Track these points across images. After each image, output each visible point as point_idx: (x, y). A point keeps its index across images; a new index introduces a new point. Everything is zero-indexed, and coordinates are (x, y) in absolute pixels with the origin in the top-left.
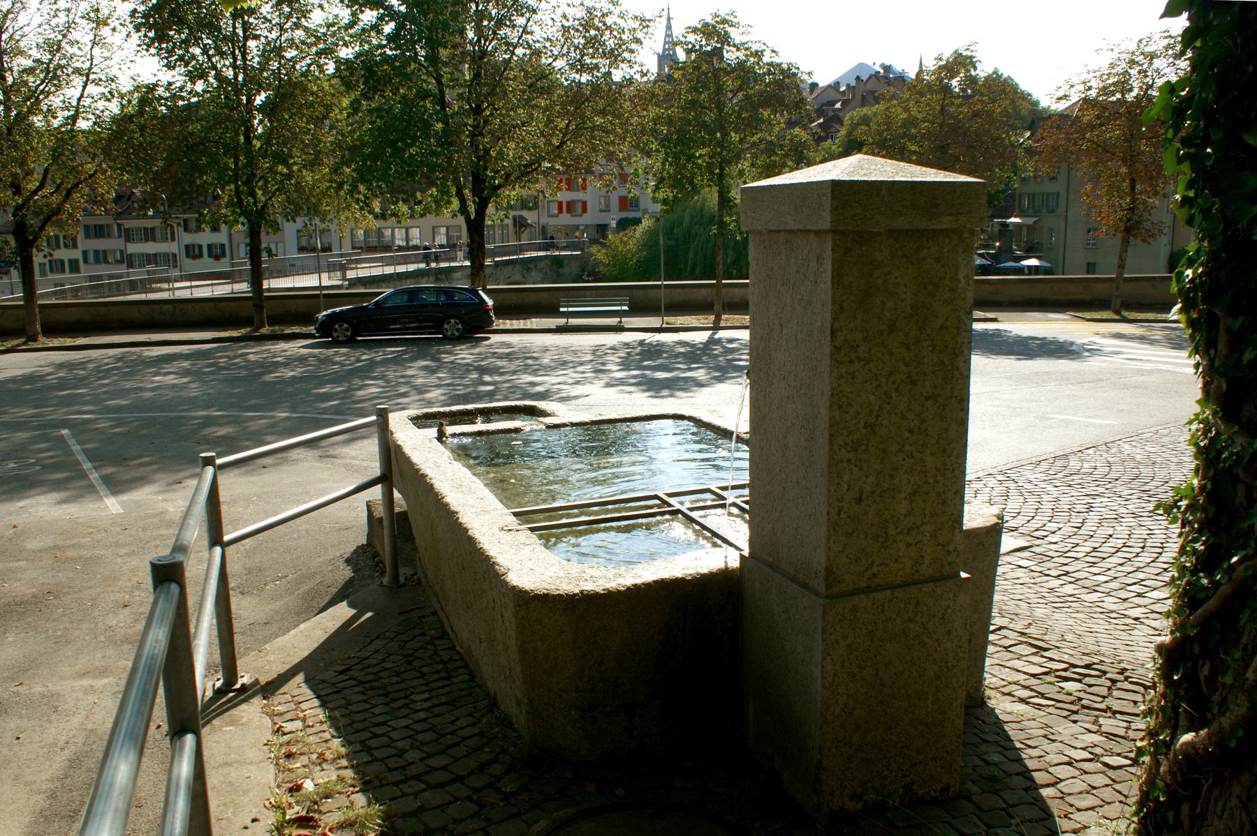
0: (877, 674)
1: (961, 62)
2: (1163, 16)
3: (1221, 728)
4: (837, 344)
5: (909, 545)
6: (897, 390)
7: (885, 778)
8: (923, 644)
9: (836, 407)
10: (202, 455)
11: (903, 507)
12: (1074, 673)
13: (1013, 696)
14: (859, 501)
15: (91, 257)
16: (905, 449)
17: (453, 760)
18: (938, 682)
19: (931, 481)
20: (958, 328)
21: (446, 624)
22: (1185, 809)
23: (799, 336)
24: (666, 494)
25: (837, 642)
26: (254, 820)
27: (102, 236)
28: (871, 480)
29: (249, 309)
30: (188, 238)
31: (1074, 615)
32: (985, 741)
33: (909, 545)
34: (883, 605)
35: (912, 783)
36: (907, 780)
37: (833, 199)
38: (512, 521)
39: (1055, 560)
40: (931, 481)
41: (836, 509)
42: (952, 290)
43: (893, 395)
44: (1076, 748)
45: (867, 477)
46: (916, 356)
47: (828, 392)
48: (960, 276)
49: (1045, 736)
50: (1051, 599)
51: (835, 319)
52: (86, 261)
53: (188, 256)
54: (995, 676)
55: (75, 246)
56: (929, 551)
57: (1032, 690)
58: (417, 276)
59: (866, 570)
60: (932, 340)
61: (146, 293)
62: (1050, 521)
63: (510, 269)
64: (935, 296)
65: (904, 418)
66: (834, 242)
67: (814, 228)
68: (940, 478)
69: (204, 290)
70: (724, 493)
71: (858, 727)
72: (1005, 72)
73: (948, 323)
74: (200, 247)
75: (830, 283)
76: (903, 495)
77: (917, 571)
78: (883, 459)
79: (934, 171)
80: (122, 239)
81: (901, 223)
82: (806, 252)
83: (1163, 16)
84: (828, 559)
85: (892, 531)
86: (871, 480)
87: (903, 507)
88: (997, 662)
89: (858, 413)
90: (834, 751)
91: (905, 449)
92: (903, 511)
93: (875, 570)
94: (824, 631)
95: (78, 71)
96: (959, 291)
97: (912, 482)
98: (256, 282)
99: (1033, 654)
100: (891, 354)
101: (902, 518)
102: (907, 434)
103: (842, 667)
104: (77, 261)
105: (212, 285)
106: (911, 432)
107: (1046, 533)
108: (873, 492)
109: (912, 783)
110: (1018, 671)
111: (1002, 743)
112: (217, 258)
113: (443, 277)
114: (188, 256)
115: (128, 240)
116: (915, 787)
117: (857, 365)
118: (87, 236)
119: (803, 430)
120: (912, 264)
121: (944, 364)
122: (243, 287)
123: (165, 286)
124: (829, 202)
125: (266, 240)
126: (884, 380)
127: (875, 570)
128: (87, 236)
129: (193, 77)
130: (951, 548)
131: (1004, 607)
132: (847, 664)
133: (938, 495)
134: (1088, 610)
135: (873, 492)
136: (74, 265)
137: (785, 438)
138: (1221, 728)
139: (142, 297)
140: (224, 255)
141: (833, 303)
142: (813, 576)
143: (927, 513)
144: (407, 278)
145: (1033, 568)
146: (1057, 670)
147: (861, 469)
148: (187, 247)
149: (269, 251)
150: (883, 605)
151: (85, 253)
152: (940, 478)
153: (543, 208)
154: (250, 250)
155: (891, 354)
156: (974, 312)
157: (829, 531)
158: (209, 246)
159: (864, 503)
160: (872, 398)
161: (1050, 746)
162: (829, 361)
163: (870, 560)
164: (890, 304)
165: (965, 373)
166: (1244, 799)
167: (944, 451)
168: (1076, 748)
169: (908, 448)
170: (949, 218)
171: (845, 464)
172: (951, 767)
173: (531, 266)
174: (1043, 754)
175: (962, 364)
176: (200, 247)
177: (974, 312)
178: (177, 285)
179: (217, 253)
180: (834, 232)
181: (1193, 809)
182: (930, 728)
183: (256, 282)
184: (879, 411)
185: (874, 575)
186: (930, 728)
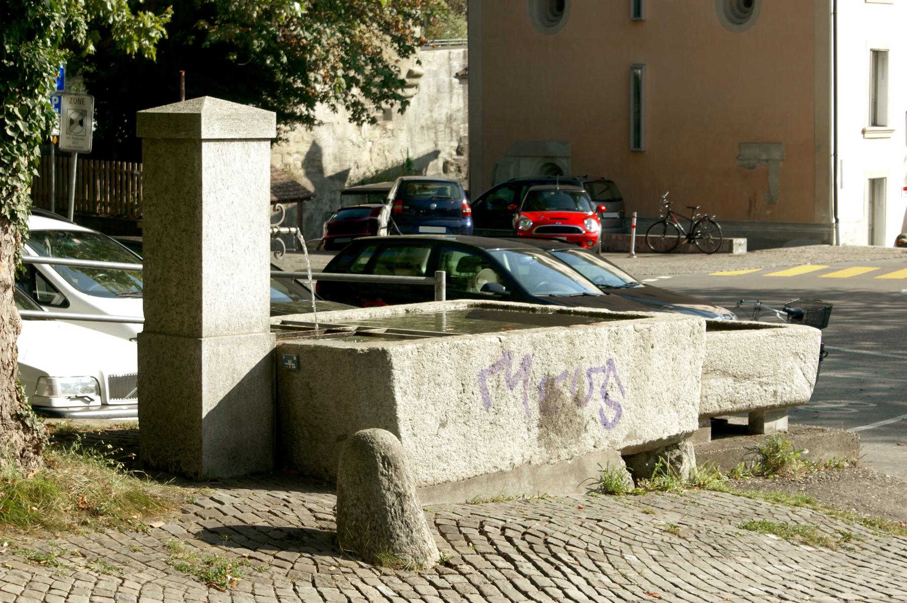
5: (177, 313)
8: (181, 373)
14: (155, 281)
21: (46, 311)
26: (292, 510)
28: (159, 271)
42: (192, 172)
48: (196, 165)
65: (173, 240)
68: (190, 278)
76: (174, 284)
87: (174, 290)
100: (167, 204)
102: (174, 249)
117: (153, 208)
130: (197, 321)
152: (190, 278)
155: (167, 204)
156: (747, 423)
170: (184, 133)
177: (747, 423)
185: (163, 326)
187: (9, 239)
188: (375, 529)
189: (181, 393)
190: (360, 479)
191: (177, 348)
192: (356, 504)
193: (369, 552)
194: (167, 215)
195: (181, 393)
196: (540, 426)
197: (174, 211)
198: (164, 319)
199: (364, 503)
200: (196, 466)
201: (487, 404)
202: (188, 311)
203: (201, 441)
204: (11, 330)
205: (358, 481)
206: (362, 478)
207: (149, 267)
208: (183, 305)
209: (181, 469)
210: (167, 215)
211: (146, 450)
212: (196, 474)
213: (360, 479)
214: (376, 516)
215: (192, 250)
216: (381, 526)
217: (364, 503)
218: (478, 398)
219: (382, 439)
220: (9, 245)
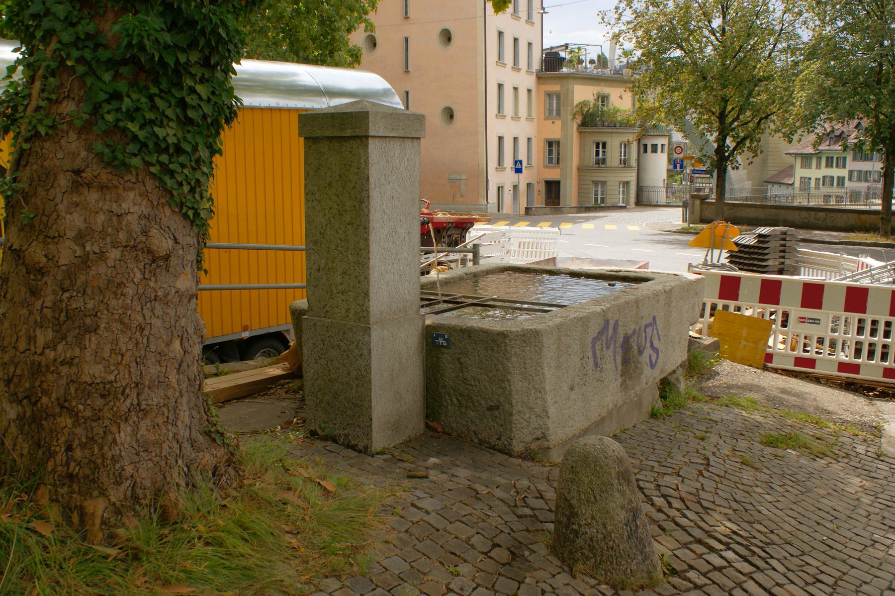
5: (343, 300)
14: (318, 270)
15: (855, 175)
17: (669, 498)
33: (343, 300)
48: (362, 161)
52: (850, 179)
55: (844, 166)
68: (356, 268)
81: (328, 133)
87: (339, 279)
100: (330, 199)
102: (339, 241)
104: (843, 178)
118: (854, 159)
127: (328, 309)
130: (364, 309)
136: (841, 181)
147: (319, 254)
151: (851, 172)
152: (356, 268)
155: (330, 199)
159: (321, 273)
160: (323, 220)
169: (339, 248)
187: (191, 243)
188: (612, 549)
189: (348, 374)
190: (595, 497)
191: (344, 333)
192: (590, 524)
193: (606, 574)
194: (330, 209)
195: (348, 374)
196: (621, 376)
197: (338, 205)
198: (328, 305)
199: (600, 523)
200: (365, 441)
201: (596, 365)
202: (355, 299)
203: (371, 419)
204: (196, 341)
205: (593, 499)
206: (598, 496)
207: (313, 257)
208: (349, 293)
209: (350, 441)
210: (330, 209)
211: (313, 421)
212: (366, 448)
213: (595, 497)
214: (613, 535)
215: (358, 243)
216: (618, 546)
217: (600, 523)
218: (591, 361)
219: (614, 451)
220: (191, 248)
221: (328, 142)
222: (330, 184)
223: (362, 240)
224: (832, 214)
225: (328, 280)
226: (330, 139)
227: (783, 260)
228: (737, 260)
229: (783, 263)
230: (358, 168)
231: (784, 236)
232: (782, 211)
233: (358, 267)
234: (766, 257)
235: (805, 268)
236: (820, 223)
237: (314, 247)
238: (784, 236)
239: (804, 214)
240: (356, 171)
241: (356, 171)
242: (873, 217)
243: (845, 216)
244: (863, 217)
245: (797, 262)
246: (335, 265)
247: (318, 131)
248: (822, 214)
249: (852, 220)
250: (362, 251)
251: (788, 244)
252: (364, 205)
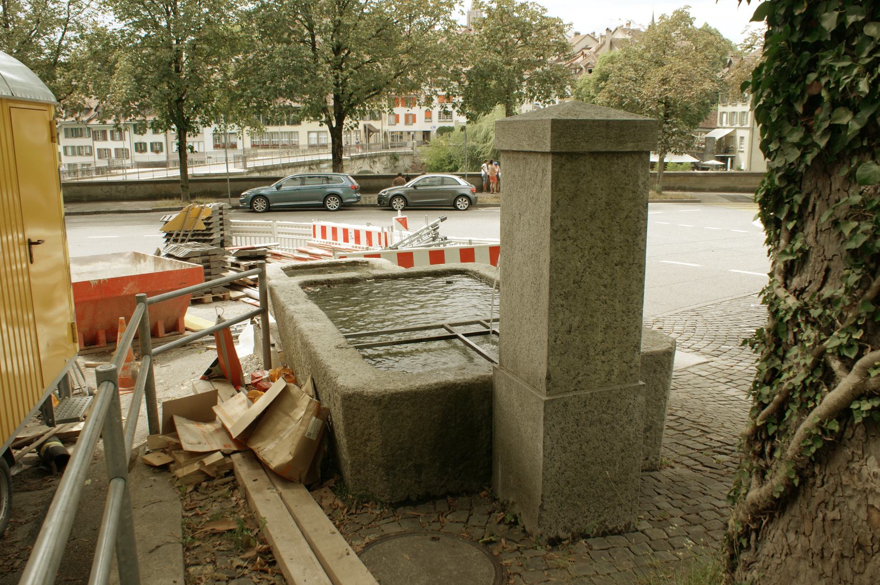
0: (581, 448)
1: (682, 18)
2: (752, 20)
3: (772, 485)
4: (555, 228)
6: (595, 259)
7: (586, 517)
9: (554, 270)
10: (137, 295)
11: (599, 337)
12: (726, 449)
13: (683, 464)
15: (69, 150)
16: (601, 298)
18: (623, 454)
19: (619, 319)
20: (638, 218)
22: (753, 536)
23: (531, 222)
24: (450, 325)
25: (554, 426)
27: (77, 136)
28: (578, 318)
29: (178, 189)
30: (138, 138)
31: (732, 410)
32: (659, 494)
33: (603, 362)
34: (585, 402)
35: (605, 521)
36: (602, 518)
37: (552, 131)
38: (342, 341)
39: (725, 371)
40: (619, 319)
41: (553, 337)
43: (593, 262)
44: (720, 500)
45: (574, 316)
46: (609, 236)
47: (548, 260)
48: (640, 183)
49: (700, 492)
50: (720, 399)
51: (553, 211)
52: (66, 154)
53: (137, 150)
54: (672, 451)
56: (617, 367)
57: (696, 460)
58: (296, 166)
59: (574, 378)
60: (620, 226)
61: (107, 176)
62: (723, 344)
63: (361, 161)
64: (622, 196)
65: (600, 277)
66: (553, 161)
67: (540, 150)
68: (625, 318)
69: (147, 175)
70: (488, 324)
71: (568, 483)
72: (713, 25)
73: (631, 214)
74: (145, 144)
75: (550, 187)
76: (599, 329)
77: (609, 380)
78: (586, 304)
79: (611, 119)
80: (91, 139)
81: (599, 147)
82: (535, 166)
83: (752, 20)
84: (548, 371)
85: (592, 353)
86: (578, 318)
87: (599, 337)
88: (675, 441)
89: (569, 274)
90: (552, 498)
91: (601, 298)
92: (600, 339)
93: (580, 378)
94: (545, 419)
95: (59, 22)
96: (638, 192)
97: (606, 320)
98: (184, 169)
99: (700, 436)
100: (592, 235)
101: (599, 344)
102: (602, 288)
103: (557, 443)
105: (153, 171)
106: (605, 286)
107: (719, 353)
108: (579, 327)
109: (605, 521)
110: (688, 447)
111: (670, 496)
112: (157, 152)
113: (314, 167)
114: (137, 150)
115: (95, 139)
116: (607, 523)
117: (569, 242)
118: (66, 137)
119: (533, 285)
120: (607, 174)
121: (628, 242)
122: (176, 173)
123: (120, 171)
124: (550, 133)
125: (190, 140)
126: (586, 252)
127: (580, 378)
128: (66, 137)
129: (138, 26)
130: (632, 364)
131: (685, 404)
132: (560, 441)
133: (624, 329)
134: (743, 406)
135: (579, 327)
137: (522, 289)
138: (772, 485)
139: (104, 179)
140: (162, 150)
141: (552, 200)
142: (539, 382)
143: (616, 341)
144: (289, 167)
145: (709, 377)
146: (715, 447)
147: (571, 311)
148: (136, 144)
149: (192, 148)
150: (585, 402)
152: (625, 318)
153: (385, 119)
154: (179, 148)
157: (548, 352)
158: (152, 144)
159: (572, 334)
160: (579, 264)
161: (702, 498)
162: (549, 240)
163: (577, 372)
164: (591, 201)
165: (642, 248)
166: (785, 531)
167: (628, 299)
168: (720, 500)
170: (632, 144)
171: (560, 308)
172: (631, 510)
173: (376, 160)
174: (697, 503)
175: (640, 242)
176: (145, 144)
178: (128, 171)
179: (157, 148)
180: (553, 153)
181: (757, 536)
182: (617, 485)
183: (184, 169)
184: (583, 273)
185: (579, 382)
186: (617, 485)
198: (582, 374)
202: (621, 356)
207: (561, 316)
221: (592, 159)
222: (592, 216)
223: (635, 282)
224: (131, 187)
225: (583, 341)
226: (596, 154)
227: (222, 232)
228: (201, 238)
229: (222, 235)
230: (634, 192)
231: (221, 211)
232: (85, 188)
233: (627, 316)
234: (211, 232)
235: (236, 236)
236: (121, 195)
237: (564, 303)
238: (221, 211)
239: (106, 188)
240: (631, 195)
241: (631, 195)
242: (167, 185)
243: (142, 187)
244: (159, 186)
245: (232, 232)
246: (595, 320)
247: (583, 144)
248: (122, 187)
249: (150, 189)
250: (634, 296)
251: (225, 217)
252: (640, 238)
